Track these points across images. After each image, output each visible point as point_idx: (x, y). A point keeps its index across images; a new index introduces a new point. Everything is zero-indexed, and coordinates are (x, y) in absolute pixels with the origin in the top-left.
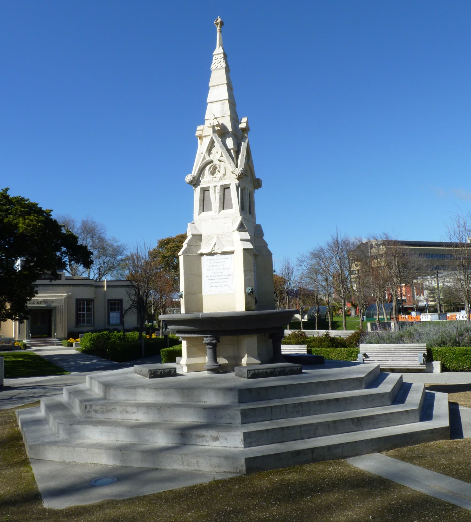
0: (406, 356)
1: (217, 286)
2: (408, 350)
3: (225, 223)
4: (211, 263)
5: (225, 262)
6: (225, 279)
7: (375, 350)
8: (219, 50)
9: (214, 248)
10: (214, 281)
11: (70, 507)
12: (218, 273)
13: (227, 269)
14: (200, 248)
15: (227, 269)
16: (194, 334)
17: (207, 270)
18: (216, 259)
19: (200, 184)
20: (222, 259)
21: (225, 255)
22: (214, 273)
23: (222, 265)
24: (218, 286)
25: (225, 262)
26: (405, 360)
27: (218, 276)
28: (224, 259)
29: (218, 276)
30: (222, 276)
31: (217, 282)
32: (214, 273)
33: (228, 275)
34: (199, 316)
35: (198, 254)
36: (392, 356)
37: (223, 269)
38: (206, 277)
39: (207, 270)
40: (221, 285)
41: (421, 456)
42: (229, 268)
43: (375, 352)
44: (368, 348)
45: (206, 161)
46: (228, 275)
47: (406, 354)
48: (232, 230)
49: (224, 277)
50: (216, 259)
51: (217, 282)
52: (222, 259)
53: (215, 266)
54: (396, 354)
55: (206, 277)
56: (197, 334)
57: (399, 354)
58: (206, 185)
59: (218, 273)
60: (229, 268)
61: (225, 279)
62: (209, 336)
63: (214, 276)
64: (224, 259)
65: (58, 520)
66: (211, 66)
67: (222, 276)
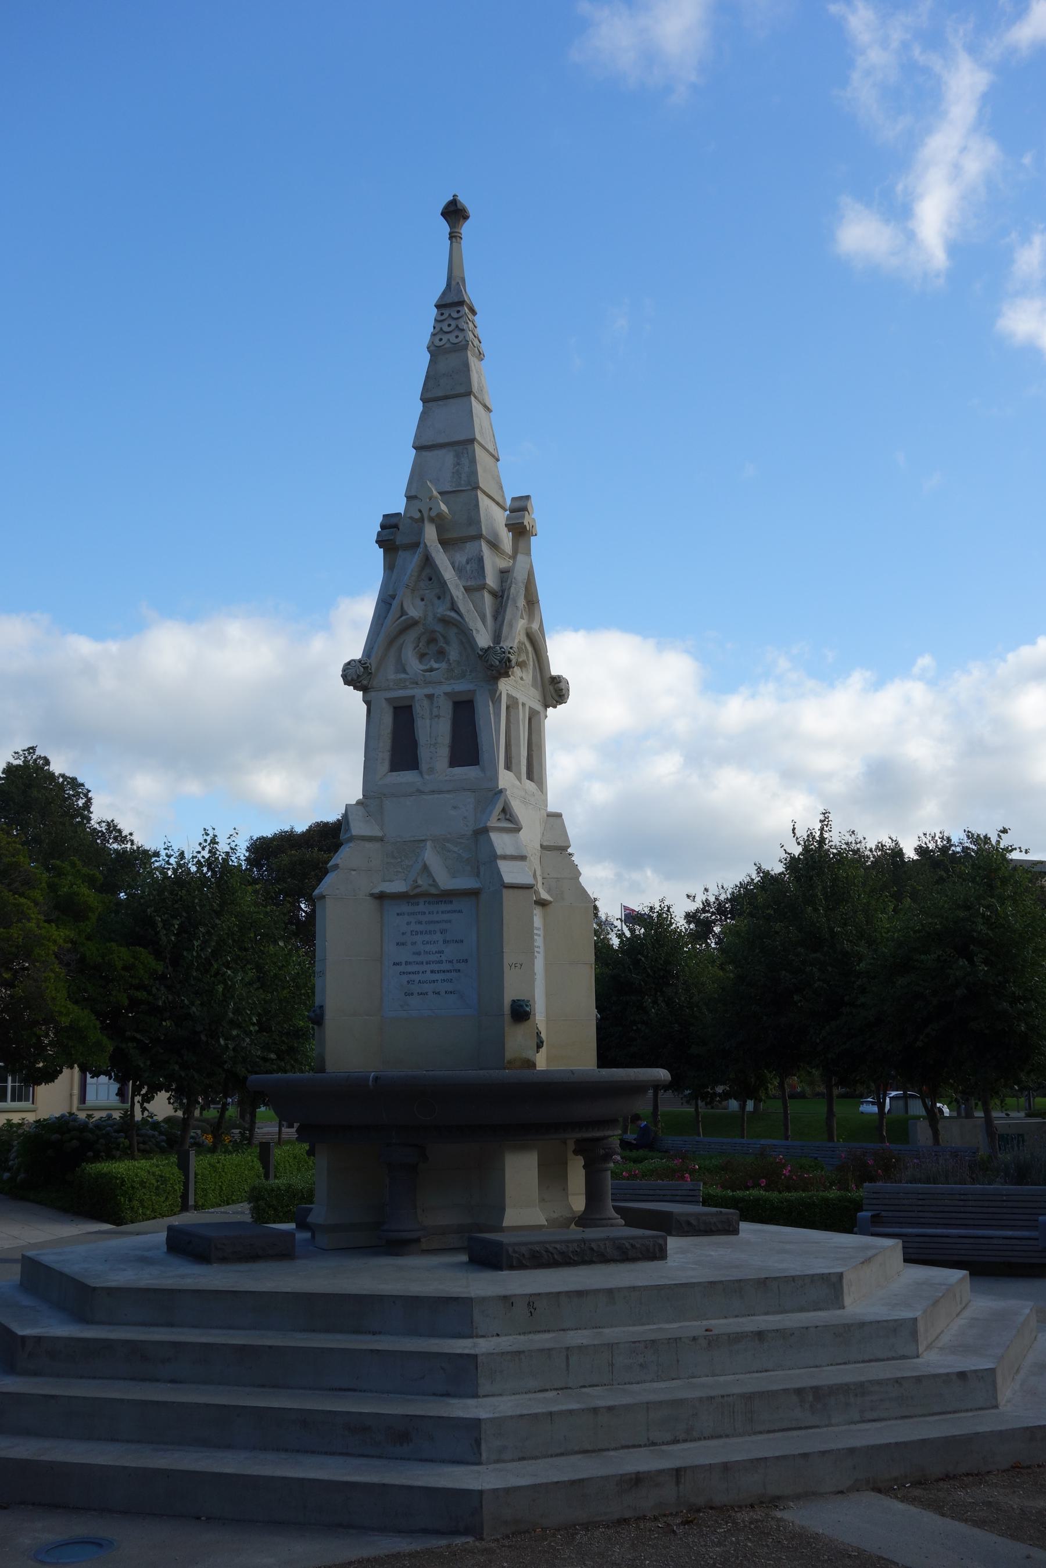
59: (426, 952)
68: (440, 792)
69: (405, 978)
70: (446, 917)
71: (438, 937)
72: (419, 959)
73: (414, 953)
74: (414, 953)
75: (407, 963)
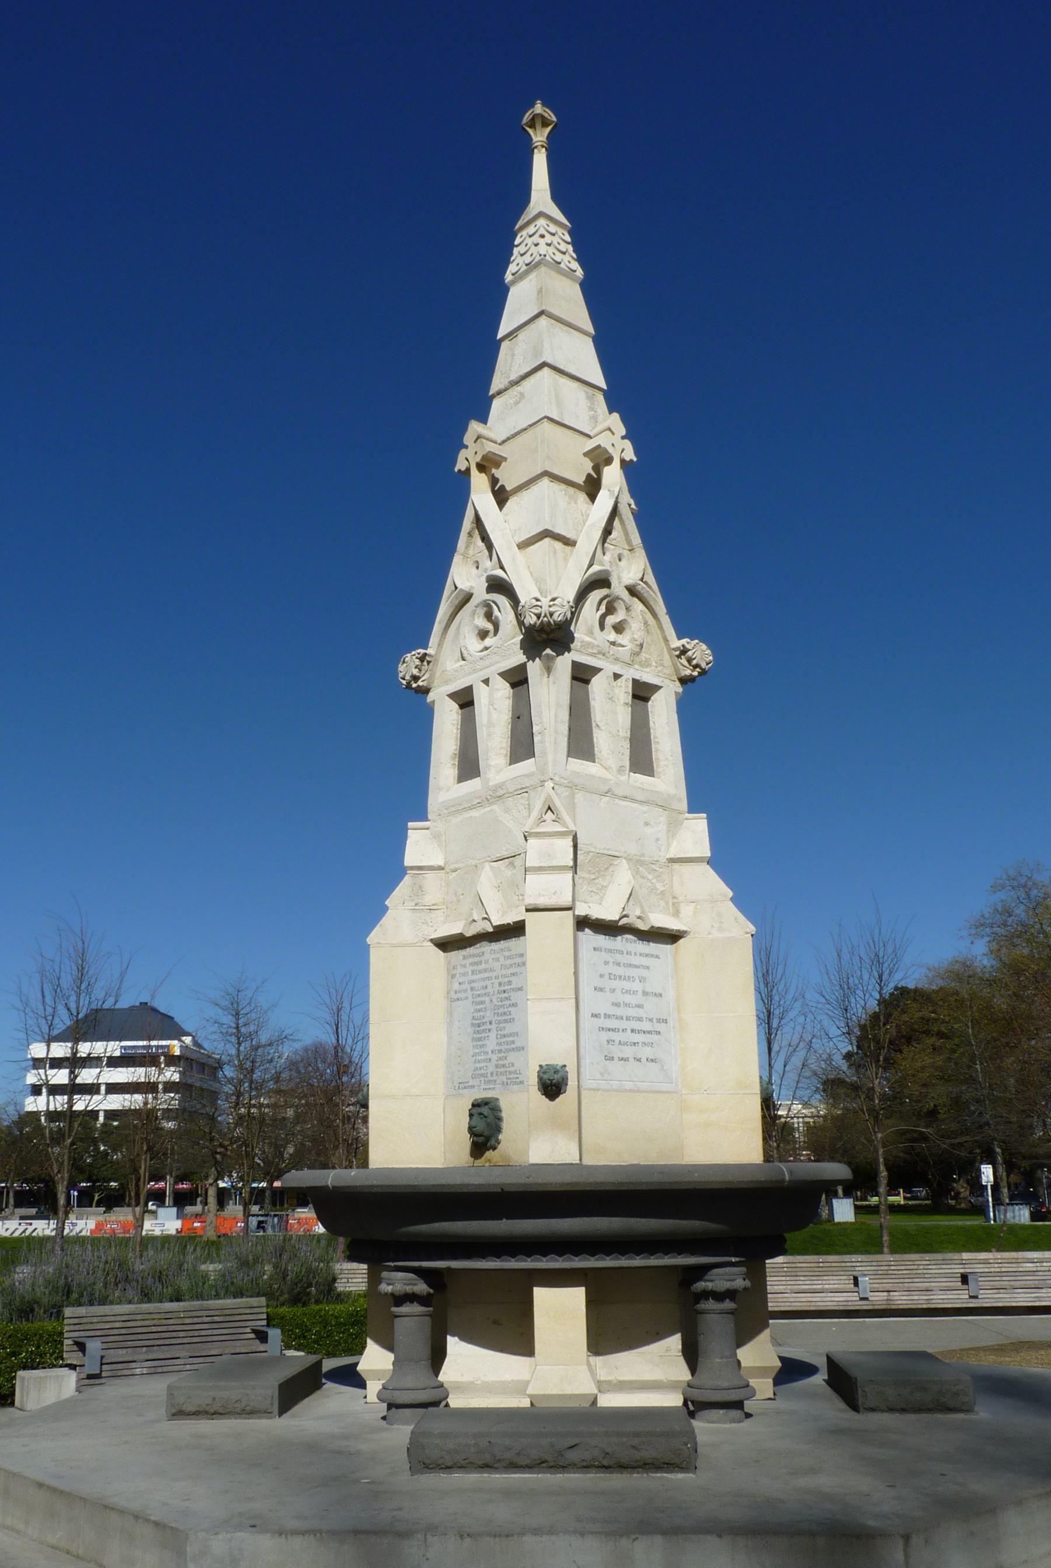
0: (210, 1339)
1: (625, 1056)
2: (216, 1319)
3: (647, 824)
4: (606, 963)
5: (648, 968)
7: (117, 1325)
10: (616, 1037)
12: (627, 1005)
13: (655, 995)
16: (608, 1254)
19: (572, 646)
21: (648, 941)
22: (617, 1005)
23: (642, 980)
25: (648, 968)
26: (227, 1352)
27: (628, 1019)
28: (647, 955)
29: (628, 1019)
30: (640, 1019)
31: (626, 1044)
32: (617, 1005)
33: (658, 1020)
34: (327, 1182)
36: (167, 1342)
37: (645, 993)
40: (638, 1057)
42: (661, 995)
43: (115, 1332)
44: (95, 1320)
45: (595, 574)
46: (658, 1020)
47: (209, 1332)
48: (671, 855)
49: (646, 1026)
51: (626, 1044)
53: (620, 977)
54: (182, 1334)
55: (593, 1015)
56: (693, 1253)
57: (191, 1334)
58: (589, 658)
59: (627, 1005)
60: (661, 995)
62: (733, 1260)
64: (647, 955)
66: (507, 263)
67: (640, 1019)
68: (633, 800)
69: (605, 1036)
70: (645, 961)
71: (636, 986)
72: (619, 1012)
73: (614, 1004)
74: (614, 1004)
75: (606, 1016)
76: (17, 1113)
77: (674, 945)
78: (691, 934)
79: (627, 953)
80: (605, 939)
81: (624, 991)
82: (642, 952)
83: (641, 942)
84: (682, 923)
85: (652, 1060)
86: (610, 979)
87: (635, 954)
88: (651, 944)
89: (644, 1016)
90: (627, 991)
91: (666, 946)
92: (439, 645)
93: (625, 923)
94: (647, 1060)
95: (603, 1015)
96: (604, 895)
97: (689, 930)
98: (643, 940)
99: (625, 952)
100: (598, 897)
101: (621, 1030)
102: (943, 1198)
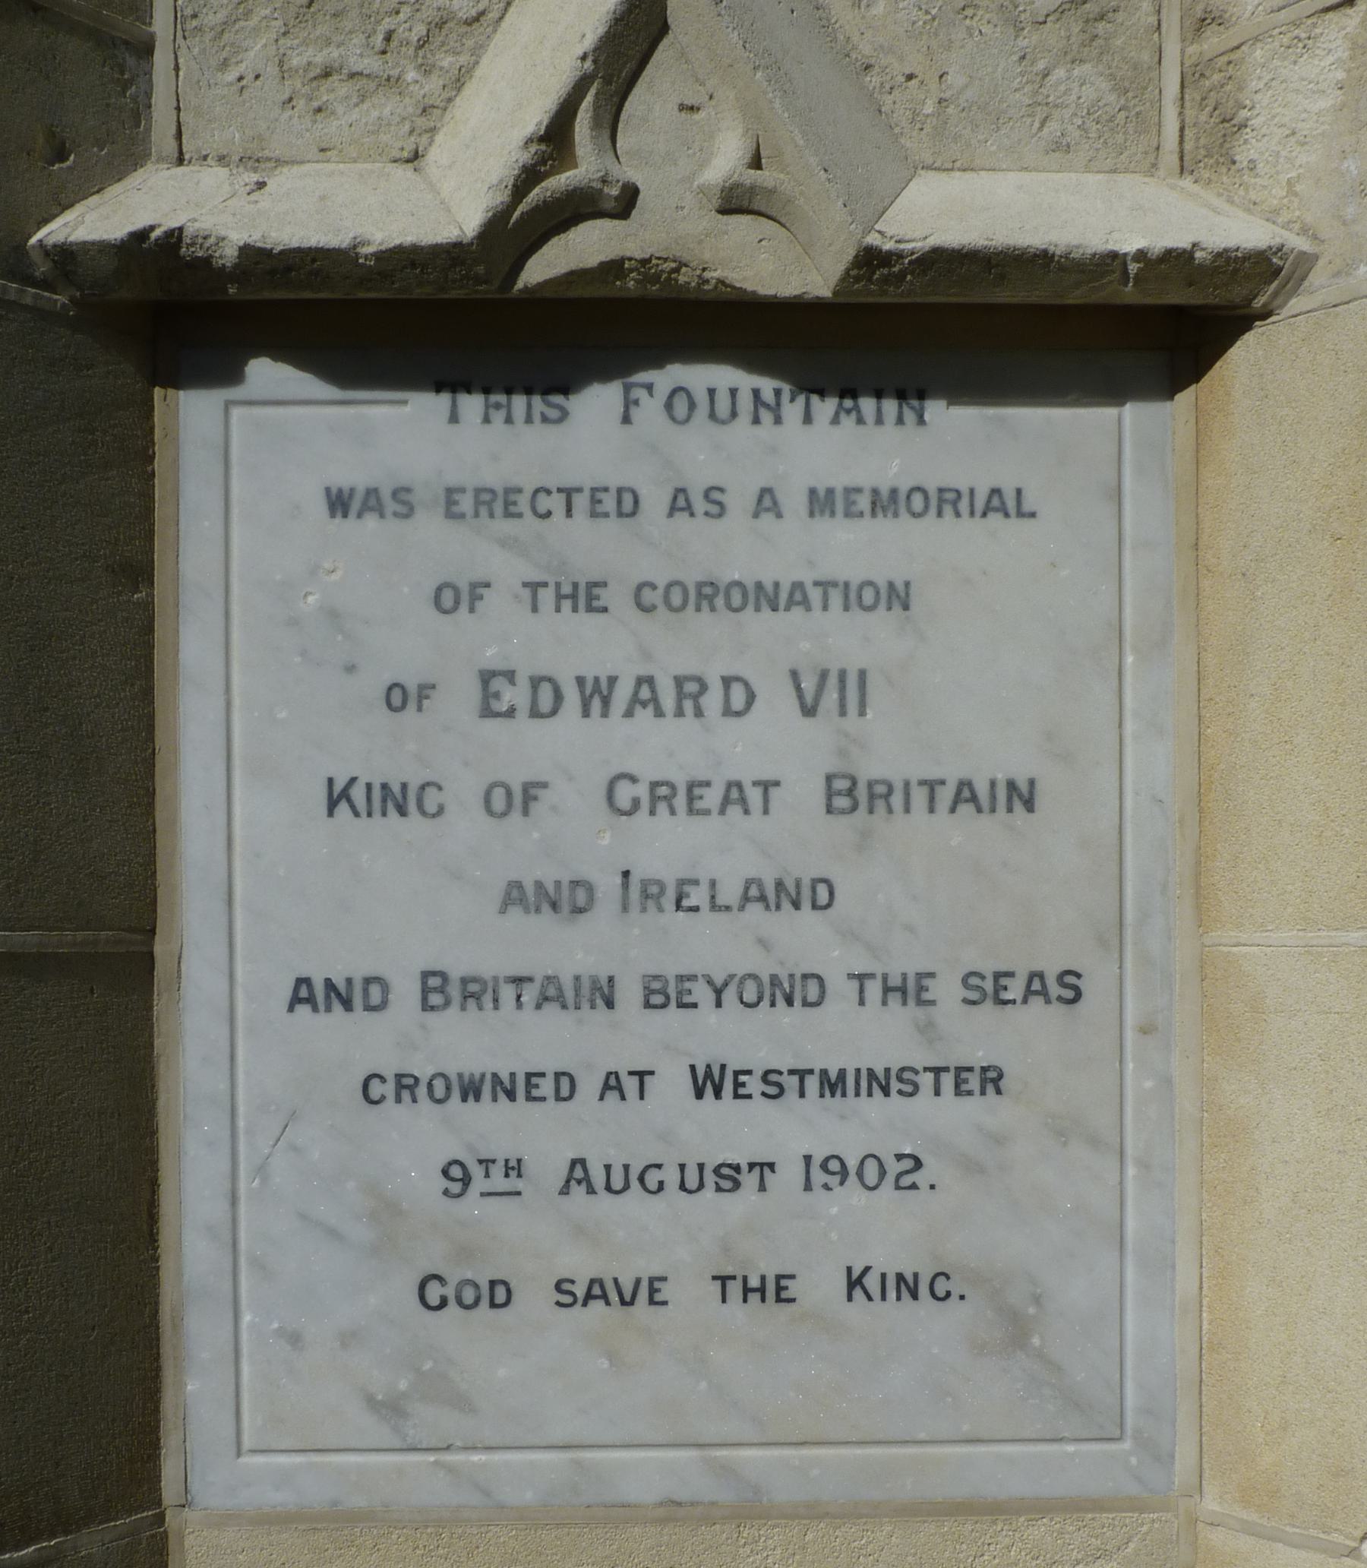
5: (898, 597)
6: (879, 1083)
8: (512, 221)
9: (610, 122)
11: (1066, 256)
14: (139, 112)
15: (965, 794)
17: (337, 798)
18: (628, 503)
20: (820, 502)
24: (653, 1290)
25: (898, 597)
35: (65, 256)
38: (302, 994)
39: (337, 798)
40: (765, 1266)
41: (11, 754)
50: (628, 503)
52: (820, 502)
55: (302, 994)
61: (879, 1083)
63: (551, 994)
65: (162, 1529)
76: (415, 146)
77: (1185, 398)
78: (1317, 277)
79: (680, 503)
80: (454, 418)
81: (624, 794)
82: (839, 481)
83: (825, 408)
84: (1251, 207)
85: (907, 1286)
86: (487, 712)
87: (767, 502)
88: (936, 409)
89: (429, 526)
90: (661, 795)
91: (1106, 414)
92: (1103, 1509)
93: (592, 259)
94: (855, 1283)
95: (406, 991)
96: (459, 82)
97: (1300, 243)
98: (849, 392)
99: (654, 501)
100: (386, 107)
101: (590, 1085)
102: (227, 270)
